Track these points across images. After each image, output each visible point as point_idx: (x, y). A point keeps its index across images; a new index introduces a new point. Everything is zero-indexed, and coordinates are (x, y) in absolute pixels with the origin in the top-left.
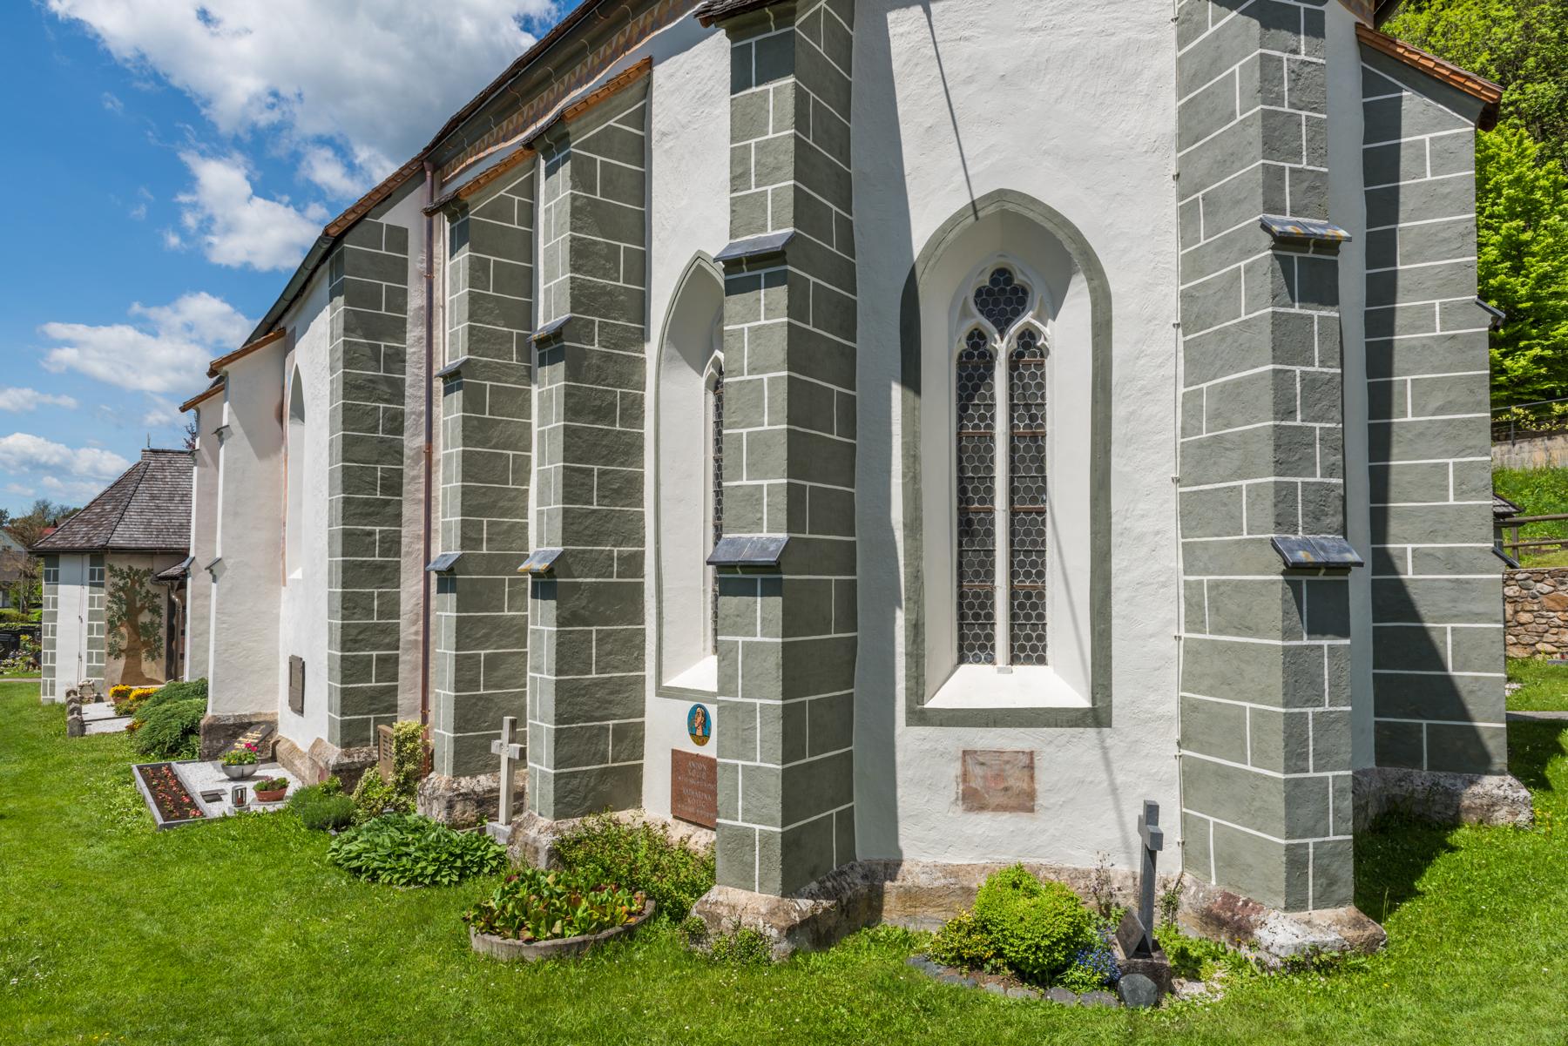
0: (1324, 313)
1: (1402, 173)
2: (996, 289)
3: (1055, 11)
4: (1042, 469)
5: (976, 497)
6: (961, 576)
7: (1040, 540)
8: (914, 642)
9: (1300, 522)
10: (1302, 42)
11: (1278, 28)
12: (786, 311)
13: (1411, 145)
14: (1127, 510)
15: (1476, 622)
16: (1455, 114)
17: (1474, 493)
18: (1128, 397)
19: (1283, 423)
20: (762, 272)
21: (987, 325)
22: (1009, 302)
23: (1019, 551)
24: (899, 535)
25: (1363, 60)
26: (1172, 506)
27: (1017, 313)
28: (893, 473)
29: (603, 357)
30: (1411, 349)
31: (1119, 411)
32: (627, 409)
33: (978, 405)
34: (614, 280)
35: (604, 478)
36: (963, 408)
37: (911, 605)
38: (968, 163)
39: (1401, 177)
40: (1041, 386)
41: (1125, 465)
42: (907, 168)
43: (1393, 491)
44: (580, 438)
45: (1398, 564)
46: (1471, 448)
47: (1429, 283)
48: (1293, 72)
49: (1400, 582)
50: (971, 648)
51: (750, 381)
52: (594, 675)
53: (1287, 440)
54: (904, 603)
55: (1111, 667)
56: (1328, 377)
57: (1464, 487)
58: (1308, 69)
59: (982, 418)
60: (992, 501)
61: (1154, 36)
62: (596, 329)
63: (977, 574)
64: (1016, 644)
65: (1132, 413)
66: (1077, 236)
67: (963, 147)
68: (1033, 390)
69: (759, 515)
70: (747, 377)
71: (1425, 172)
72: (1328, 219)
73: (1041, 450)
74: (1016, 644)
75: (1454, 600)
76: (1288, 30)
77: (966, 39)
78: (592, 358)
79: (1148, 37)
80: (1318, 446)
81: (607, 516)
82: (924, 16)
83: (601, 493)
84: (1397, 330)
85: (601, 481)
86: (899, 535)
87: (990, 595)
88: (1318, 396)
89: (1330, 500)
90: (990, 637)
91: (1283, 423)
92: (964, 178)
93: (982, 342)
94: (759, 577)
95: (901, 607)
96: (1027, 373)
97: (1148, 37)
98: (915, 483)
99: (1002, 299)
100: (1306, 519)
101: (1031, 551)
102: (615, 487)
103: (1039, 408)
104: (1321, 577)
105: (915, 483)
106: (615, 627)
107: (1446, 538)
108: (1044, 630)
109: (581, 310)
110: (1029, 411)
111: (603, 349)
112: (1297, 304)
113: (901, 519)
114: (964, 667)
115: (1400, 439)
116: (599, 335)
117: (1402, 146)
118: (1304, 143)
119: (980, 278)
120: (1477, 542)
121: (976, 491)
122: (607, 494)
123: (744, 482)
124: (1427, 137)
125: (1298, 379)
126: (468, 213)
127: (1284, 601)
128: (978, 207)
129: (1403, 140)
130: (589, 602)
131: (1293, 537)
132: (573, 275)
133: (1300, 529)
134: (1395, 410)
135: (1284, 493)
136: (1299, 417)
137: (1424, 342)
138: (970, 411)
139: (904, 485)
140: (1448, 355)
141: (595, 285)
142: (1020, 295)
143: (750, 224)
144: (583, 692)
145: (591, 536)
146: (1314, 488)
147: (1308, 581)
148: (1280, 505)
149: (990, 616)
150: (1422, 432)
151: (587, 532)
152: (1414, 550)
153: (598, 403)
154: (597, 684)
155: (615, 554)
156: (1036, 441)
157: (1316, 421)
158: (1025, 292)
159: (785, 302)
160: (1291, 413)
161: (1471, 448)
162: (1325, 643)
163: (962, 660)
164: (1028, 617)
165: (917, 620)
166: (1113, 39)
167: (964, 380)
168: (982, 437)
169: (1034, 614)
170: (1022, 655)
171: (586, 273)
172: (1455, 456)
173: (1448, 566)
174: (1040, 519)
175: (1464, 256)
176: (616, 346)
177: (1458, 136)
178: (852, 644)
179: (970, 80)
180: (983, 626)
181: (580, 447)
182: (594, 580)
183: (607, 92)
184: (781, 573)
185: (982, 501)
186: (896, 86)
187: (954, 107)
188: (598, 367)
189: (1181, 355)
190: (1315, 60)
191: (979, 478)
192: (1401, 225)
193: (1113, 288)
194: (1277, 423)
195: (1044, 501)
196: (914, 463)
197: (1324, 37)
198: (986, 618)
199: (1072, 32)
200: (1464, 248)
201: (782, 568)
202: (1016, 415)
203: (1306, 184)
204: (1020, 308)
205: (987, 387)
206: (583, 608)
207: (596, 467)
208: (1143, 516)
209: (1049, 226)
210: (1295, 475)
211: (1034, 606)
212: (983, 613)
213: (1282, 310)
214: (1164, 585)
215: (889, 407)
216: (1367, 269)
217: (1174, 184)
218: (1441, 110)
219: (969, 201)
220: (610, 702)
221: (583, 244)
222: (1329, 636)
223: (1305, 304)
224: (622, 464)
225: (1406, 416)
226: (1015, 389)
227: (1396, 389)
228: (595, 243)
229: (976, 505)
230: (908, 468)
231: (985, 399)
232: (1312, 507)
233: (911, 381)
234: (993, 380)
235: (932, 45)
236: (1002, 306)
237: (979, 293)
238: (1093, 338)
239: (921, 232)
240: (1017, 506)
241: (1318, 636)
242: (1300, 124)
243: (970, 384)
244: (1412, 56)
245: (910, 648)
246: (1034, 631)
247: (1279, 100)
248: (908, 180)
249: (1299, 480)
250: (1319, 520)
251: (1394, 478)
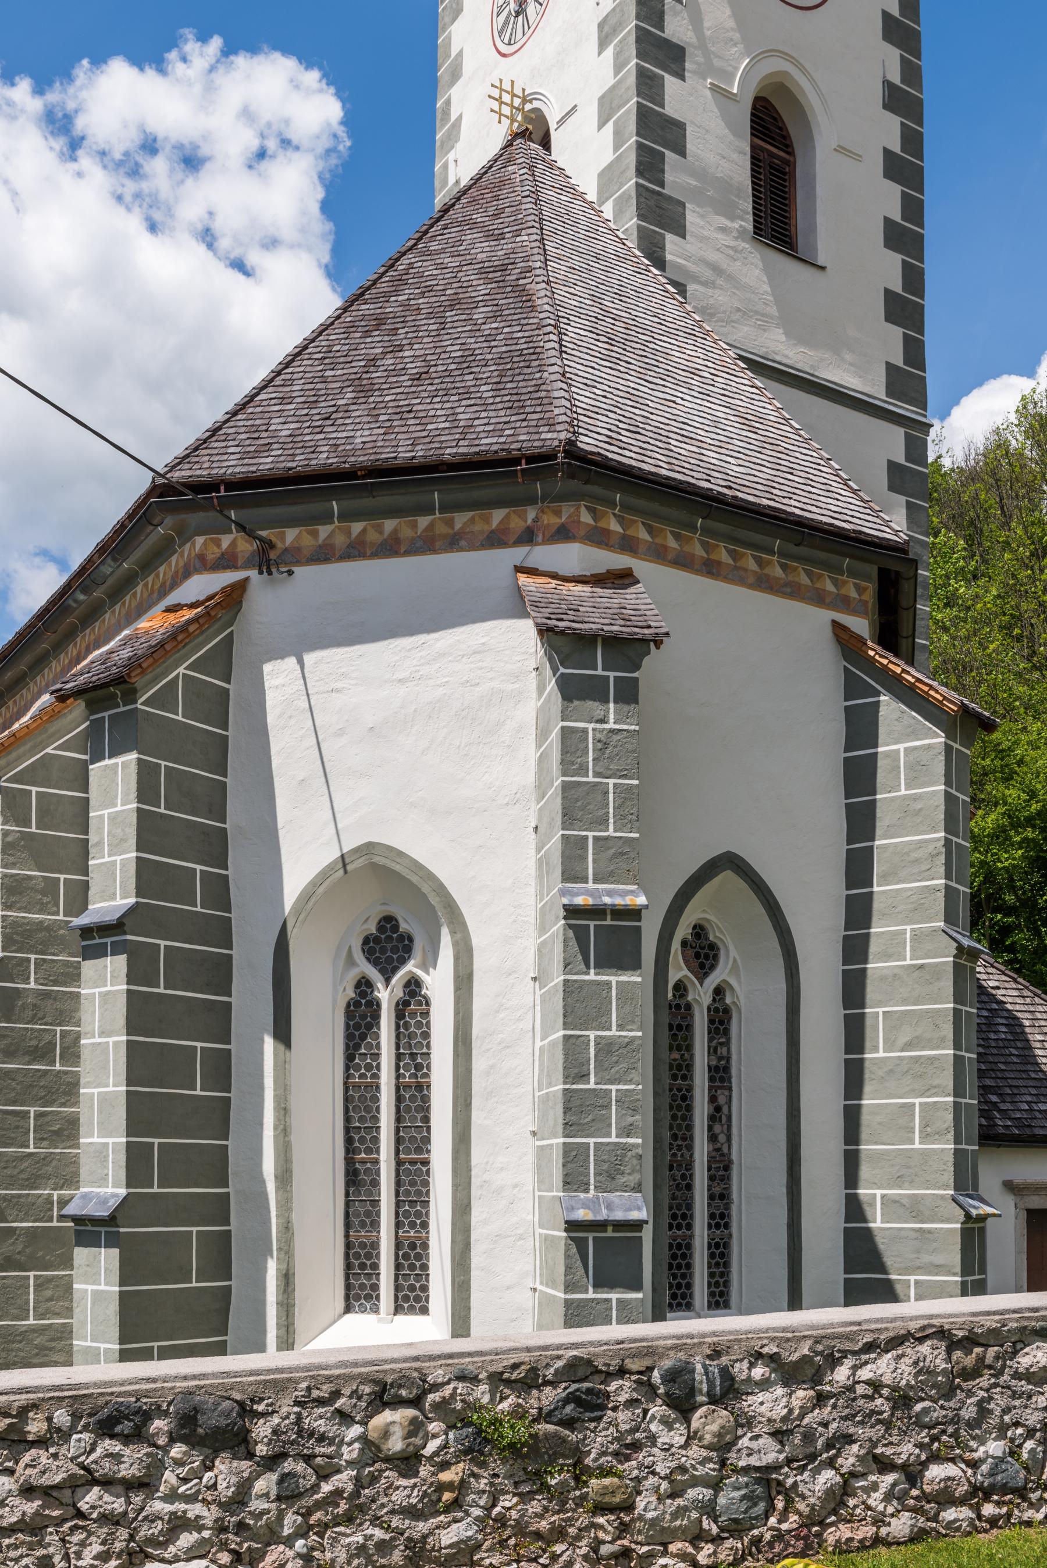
0: (624, 978)
1: (879, 785)
2: (383, 936)
3: (422, 661)
4: (426, 1119)
5: (363, 1147)
6: (348, 1225)
7: (424, 1190)
8: (285, 1291)
9: (592, 1181)
10: (612, 711)
11: (582, 698)
12: (125, 980)
13: (888, 754)
14: (487, 1163)
15: (937, 1275)
16: (927, 723)
17: (937, 1137)
18: (488, 1050)
19: (574, 1087)
20: (109, 940)
21: (373, 973)
22: (395, 949)
23: (404, 1201)
24: (271, 1187)
25: (845, 659)
26: (530, 1159)
27: (403, 961)
28: (265, 1126)
29: (40, 995)
30: (883, 979)
31: (479, 1064)
32: (68, 1048)
33: (365, 1054)
34: (53, 915)
35: (42, 1120)
36: (349, 1058)
37: (282, 1255)
38: (338, 816)
39: (878, 790)
40: (426, 1035)
41: (485, 1118)
42: (281, 822)
43: (865, 1133)
44: (13, 1080)
45: (867, 1209)
46: (935, 1087)
47: (901, 907)
48: (599, 741)
49: (869, 1229)
50: (358, 1298)
51: (100, 1043)
52: (31, 1321)
53: (578, 1103)
54: (275, 1253)
55: (469, 1318)
56: (627, 1040)
57: (928, 1129)
58: (616, 737)
59: (369, 1067)
60: (378, 1152)
61: (516, 686)
62: (32, 967)
63: (363, 1224)
64: (400, 1295)
65: (492, 1067)
66: (441, 889)
67: (334, 799)
68: (419, 1039)
69: (106, 1172)
70: (97, 1040)
71: (899, 785)
72: (637, 884)
73: (426, 1099)
74: (400, 1295)
75: (918, 1251)
76: (595, 700)
77: (338, 691)
78: (27, 996)
79: (511, 687)
80: (614, 1107)
81: (46, 1159)
82: (298, 667)
83: (38, 1136)
84: (871, 957)
85: (39, 1123)
86: (271, 1187)
87: (375, 1245)
88: (615, 1059)
89: (627, 1159)
90: (375, 1287)
91: (574, 1087)
92: (334, 831)
93: (369, 991)
94: (103, 1230)
95: (272, 1257)
96: (413, 1022)
97: (511, 687)
98: (286, 1135)
99: (389, 946)
100: (599, 1178)
101: (416, 1202)
102: (56, 1128)
103: (424, 1057)
104: (610, 1233)
105: (286, 1135)
106: (56, 1273)
107: (912, 1184)
108: (428, 1281)
109: (14, 948)
110: (414, 1060)
111: (41, 987)
112: (592, 971)
113: (272, 1171)
114: (347, 1316)
115: (873, 1076)
116: (35, 973)
117: (879, 756)
118: (611, 811)
119: (365, 926)
120: (939, 1188)
121: (362, 1140)
122: (46, 1136)
123: (95, 1140)
124: (901, 747)
125: (592, 1044)
126: (136, 702)
127: (567, 1257)
128: (347, 861)
129: (880, 749)
130: (26, 1247)
131: (582, 1195)
132: (4, 913)
133: (592, 1187)
134: (868, 1044)
135: (574, 1153)
136: (592, 1079)
137: (896, 971)
138: (357, 1061)
139: (275, 1137)
140: (916, 986)
141: (31, 922)
142: (406, 942)
143: (104, 891)
144: (18, 1338)
145: (27, 1180)
146: (608, 1148)
147: (594, 1238)
148: (569, 1166)
149: (375, 1266)
150: (894, 1069)
151: (22, 1176)
152: (883, 1197)
153: (34, 1043)
154: (34, 1330)
155: (55, 1198)
156: (421, 1091)
157: (612, 1083)
158: (411, 939)
159: (125, 970)
160: (584, 1077)
161: (935, 1087)
162: (614, 1296)
163: (348, 1309)
164: (412, 1267)
165: (288, 1270)
166: (477, 689)
167: (351, 1030)
168: (368, 1086)
169: (418, 1264)
170: (406, 1305)
171: (20, 909)
172: (921, 1096)
173: (913, 1214)
174: (424, 1169)
175: (933, 879)
176: (55, 983)
177: (929, 747)
178: (226, 1294)
179: (341, 732)
180: (369, 1276)
181: (14, 1089)
182: (30, 1224)
183: (39, 721)
184: (118, 1226)
185: (368, 1151)
186: (271, 738)
187: (325, 760)
188: (35, 1005)
189: (538, 1008)
190: (625, 727)
191: (366, 1128)
192: (877, 843)
193: (475, 941)
194: (568, 1086)
195: (428, 1151)
196: (285, 1114)
197: (636, 702)
198: (371, 1269)
199: (438, 683)
200: (933, 870)
201: (119, 1221)
202: (402, 1064)
203: (613, 851)
204: (406, 956)
205: (374, 1037)
206: (19, 1253)
207: (32, 1110)
208: (502, 1169)
209: (414, 879)
210: (587, 1136)
211: (419, 1257)
212: (368, 1263)
213: (575, 977)
214: (521, 1238)
215: (262, 1060)
216: (847, 889)
217: (533, 836)
218: (914, 718)
219: (339, 854)
220: (51, 1349)
221: (16, 880)
222: (618, 1289)
223: (601, 970)
224: (63, 1105)
225: (878, 1052)
226: (402, 1037)
227: (868, 1022)
228: (30, 877)
229: (363, 1155)
230: (279, 1120)
231: (371, 1048)
232: (605, 1166)
233: (283, 1034)
234: (379, 1029)
235: (305, 697)
236: (389, 954)
237: (366, 941)
238: (455, 991)
239: (294, 884)
240: (402, 1156)
241: (606, 1289)
242: (607, 792)
243: (357, 1033)
244: (882, 660)
245: (280, 1297)
246: (418, 1282)
247: (583, 770)
248: (281, 833)
249: (591, 1141)
250: (613, 1178)
251: (865, 1118)
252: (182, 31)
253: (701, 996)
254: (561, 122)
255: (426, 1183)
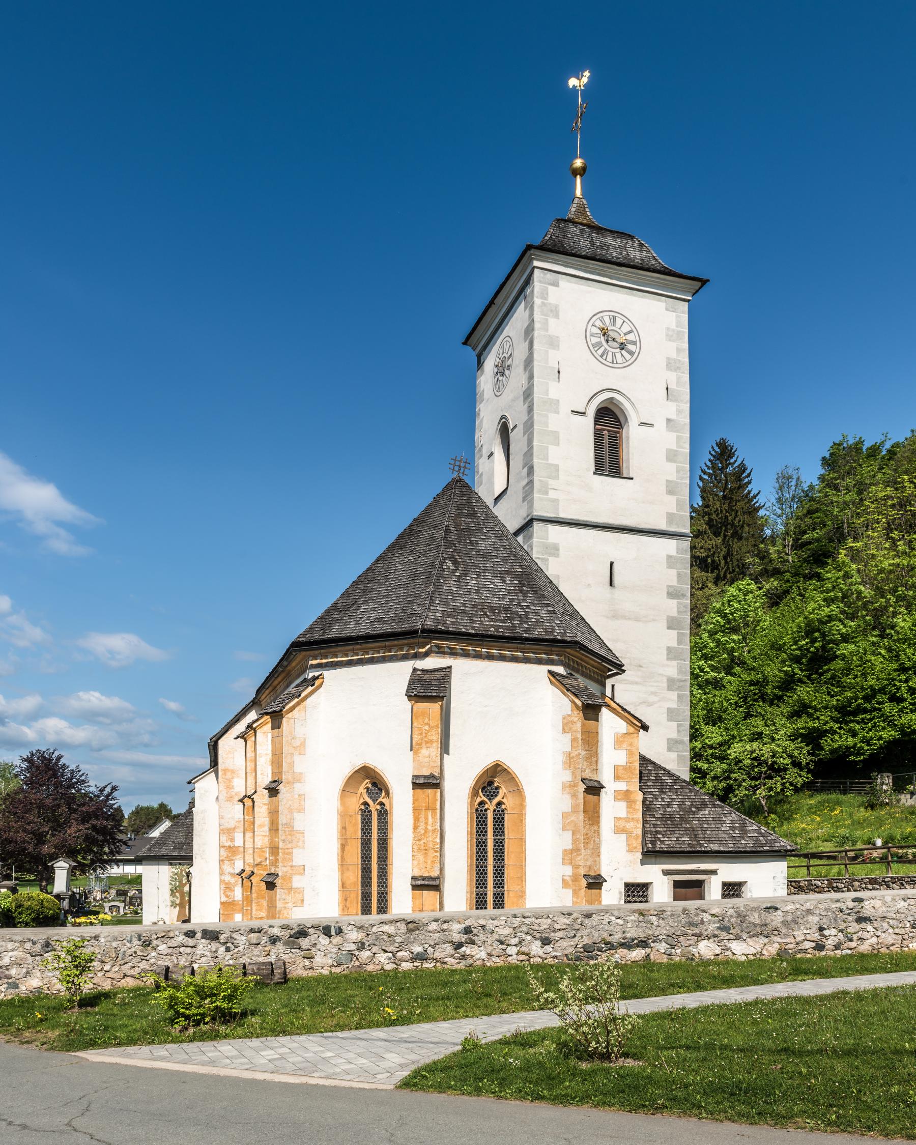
211: (385, 897)
252: (571, 87)
253: (491, 806)
254: (512, 430)
255: (387, 872)
